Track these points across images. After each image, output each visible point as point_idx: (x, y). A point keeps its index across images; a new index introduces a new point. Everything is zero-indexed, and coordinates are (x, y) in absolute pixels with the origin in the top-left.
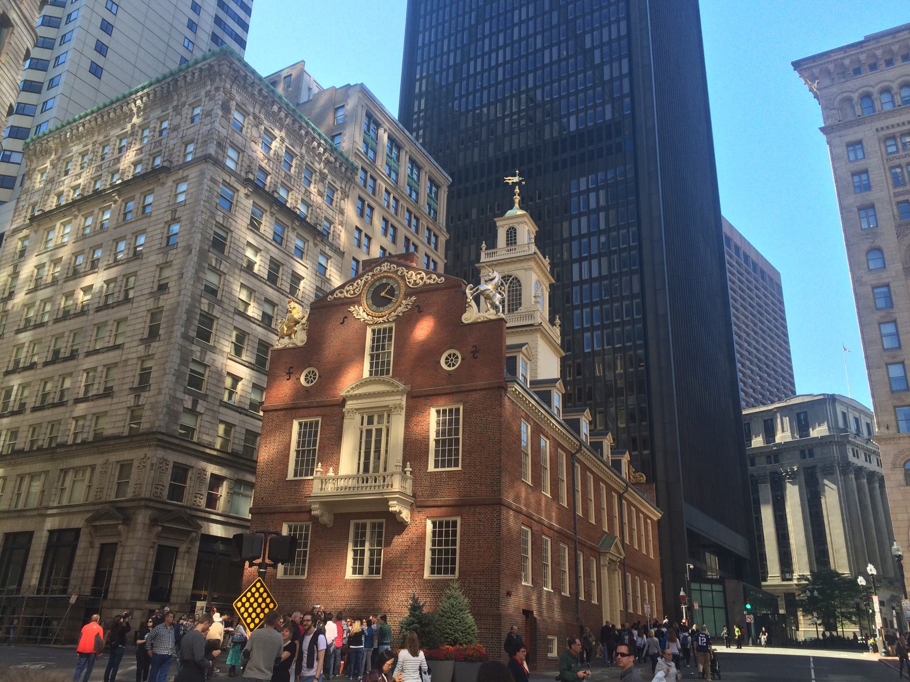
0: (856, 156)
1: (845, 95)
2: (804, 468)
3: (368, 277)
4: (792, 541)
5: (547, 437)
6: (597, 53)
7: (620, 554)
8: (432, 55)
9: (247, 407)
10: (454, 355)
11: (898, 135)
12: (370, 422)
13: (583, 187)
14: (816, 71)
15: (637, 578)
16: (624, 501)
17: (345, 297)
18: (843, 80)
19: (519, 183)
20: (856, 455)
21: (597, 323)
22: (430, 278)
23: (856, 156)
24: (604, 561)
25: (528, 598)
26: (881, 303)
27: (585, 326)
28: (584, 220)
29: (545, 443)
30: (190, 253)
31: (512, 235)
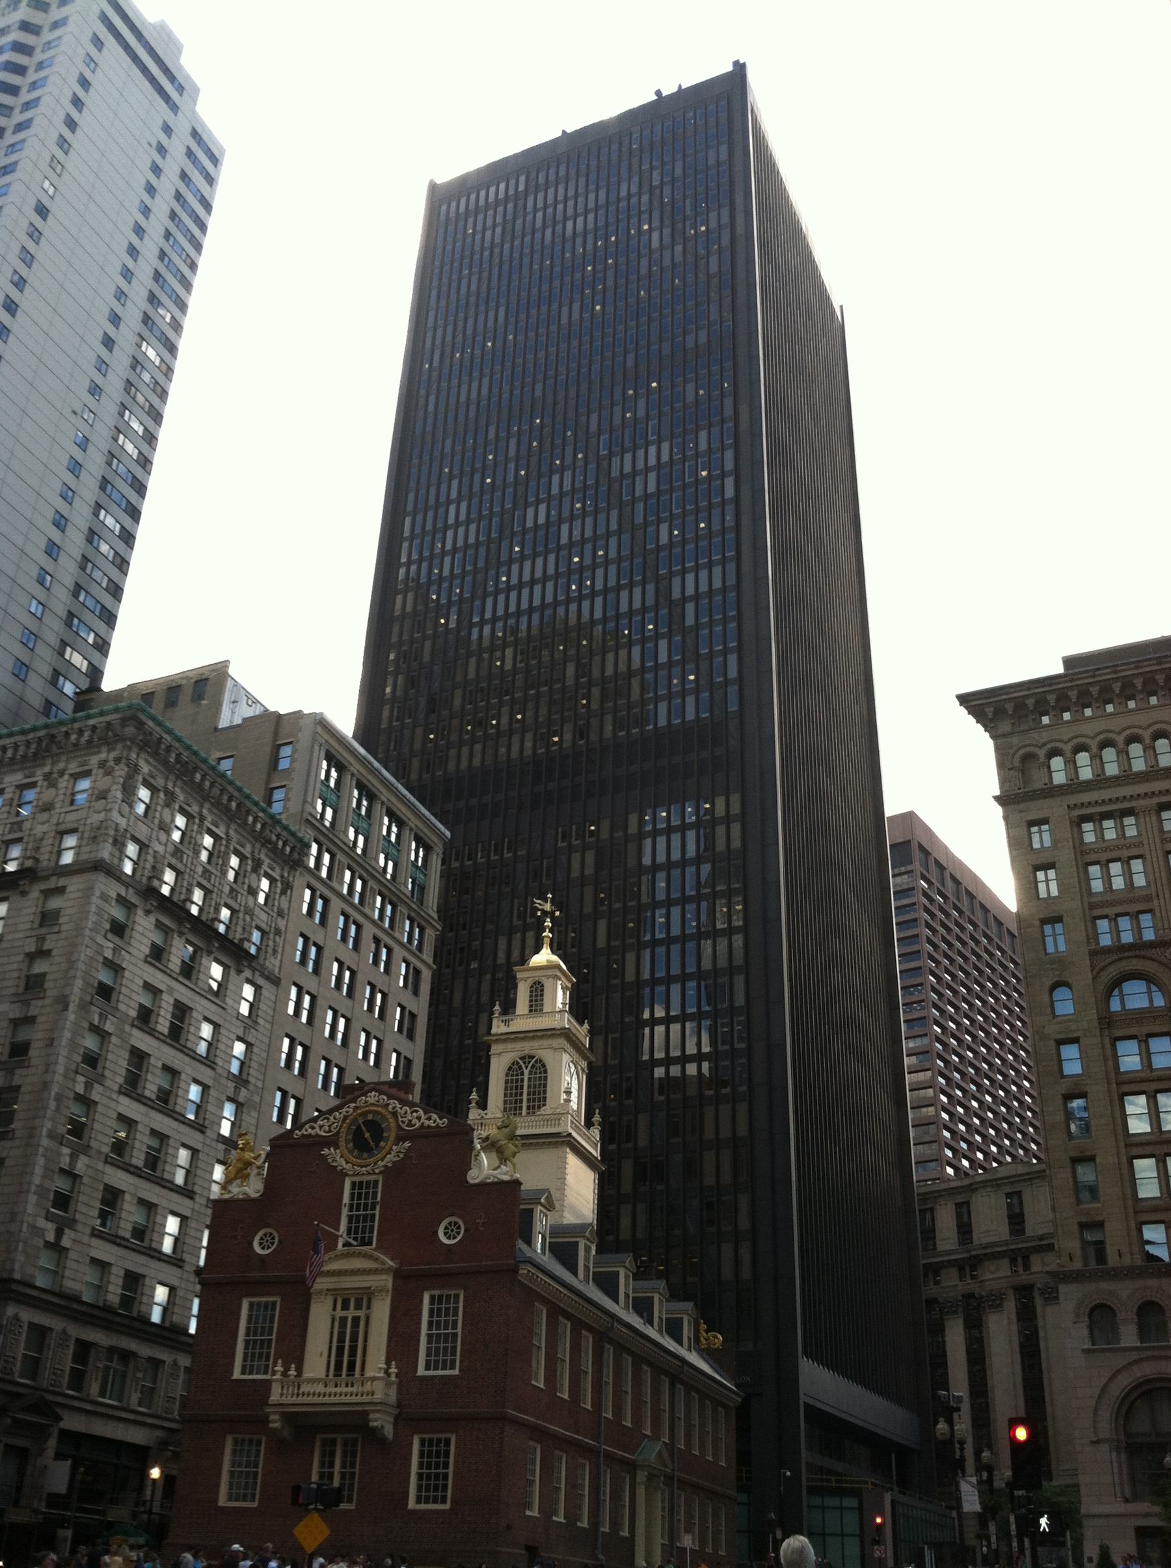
3: (349, 1109)
6: (690, 608)
9: (128, 1235)
10: (456, 1223)
12: (345, 1307)
17: (317, 1135)
22: (429, 1119)
24: (641, 1476)
30: (66, 1008)
31: (537, 991)
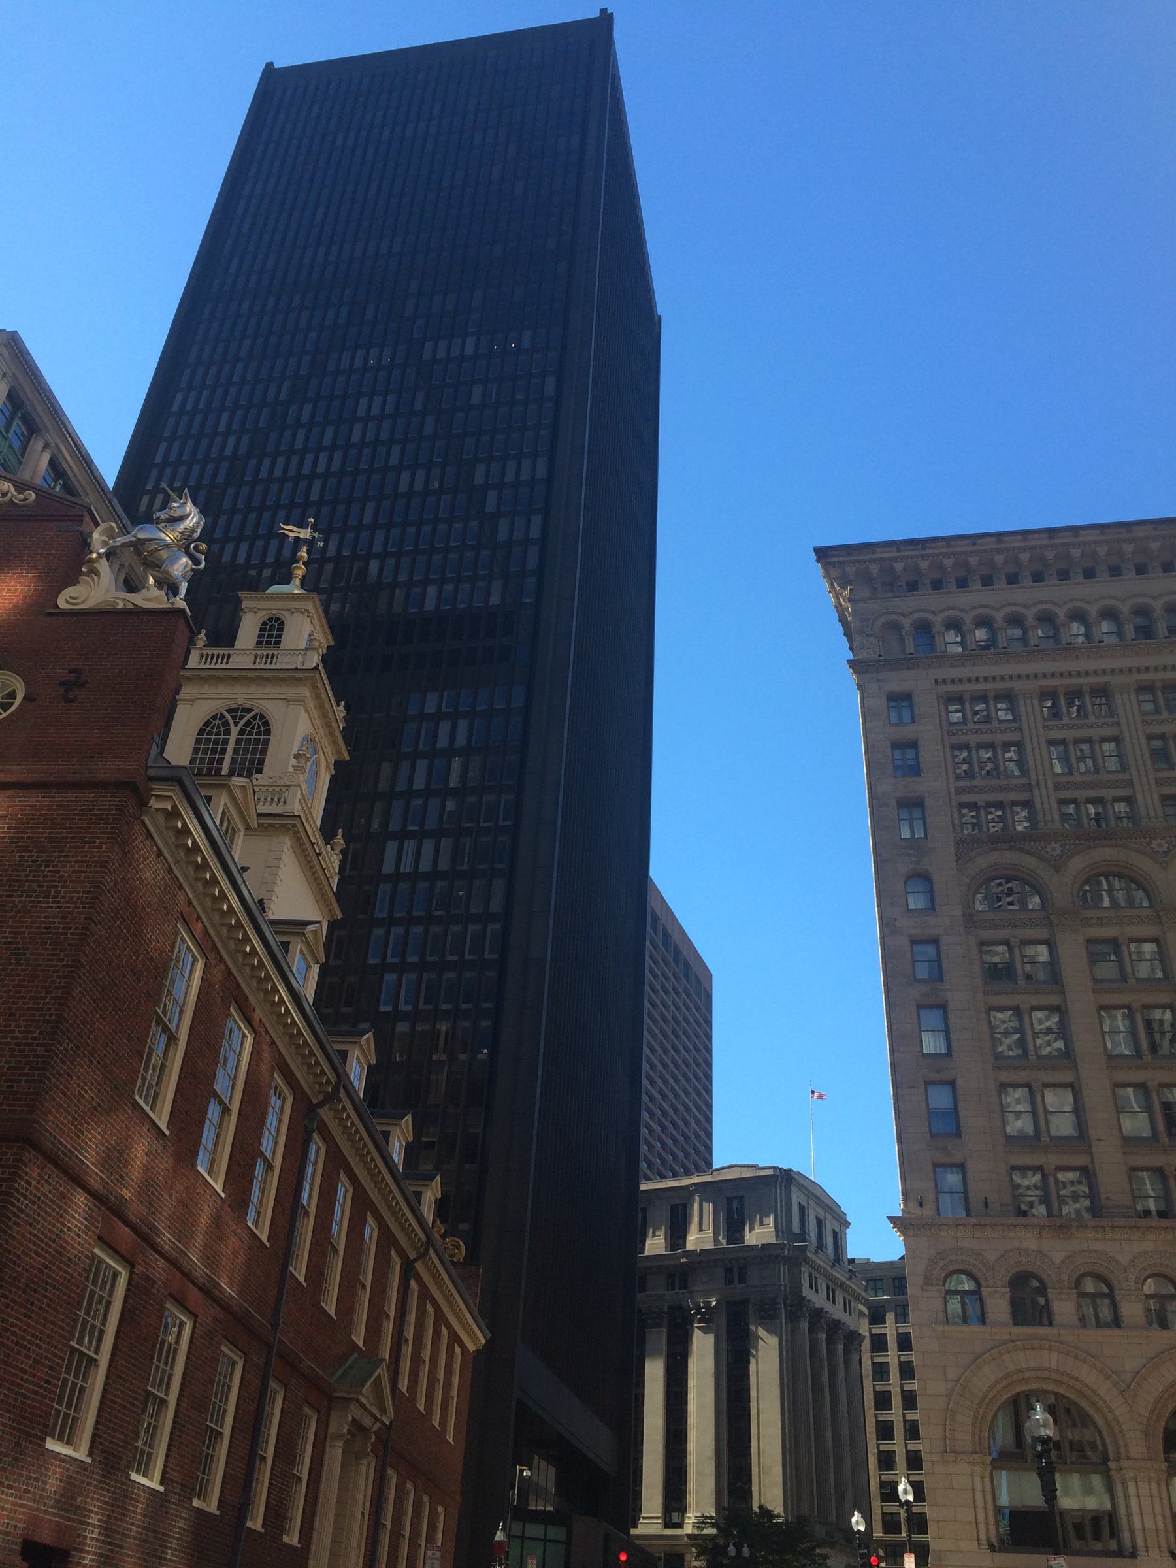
0: (900, 717)
1: (892, 617)
2: (728, 1303)
4: (692, 1446)
5: (249, 1022)
6: (492, 496)
7: (383, 1410)
8: (194, 432)
11: (967, 696)
13: (430, 708)
14: (850, 570)
15: (409, 1486)
16: (413, 1283)
18: (891, 595)
19: (310, 543)
20: (814, 1286)
21: (412, 959)
23: (900, 717)
24: (339, 1424)
25: (69, 1500)
26: (922, 972)
27: (390, 960)
28: (422, 765)
29: (240, 1047)
31: (272, 632)
